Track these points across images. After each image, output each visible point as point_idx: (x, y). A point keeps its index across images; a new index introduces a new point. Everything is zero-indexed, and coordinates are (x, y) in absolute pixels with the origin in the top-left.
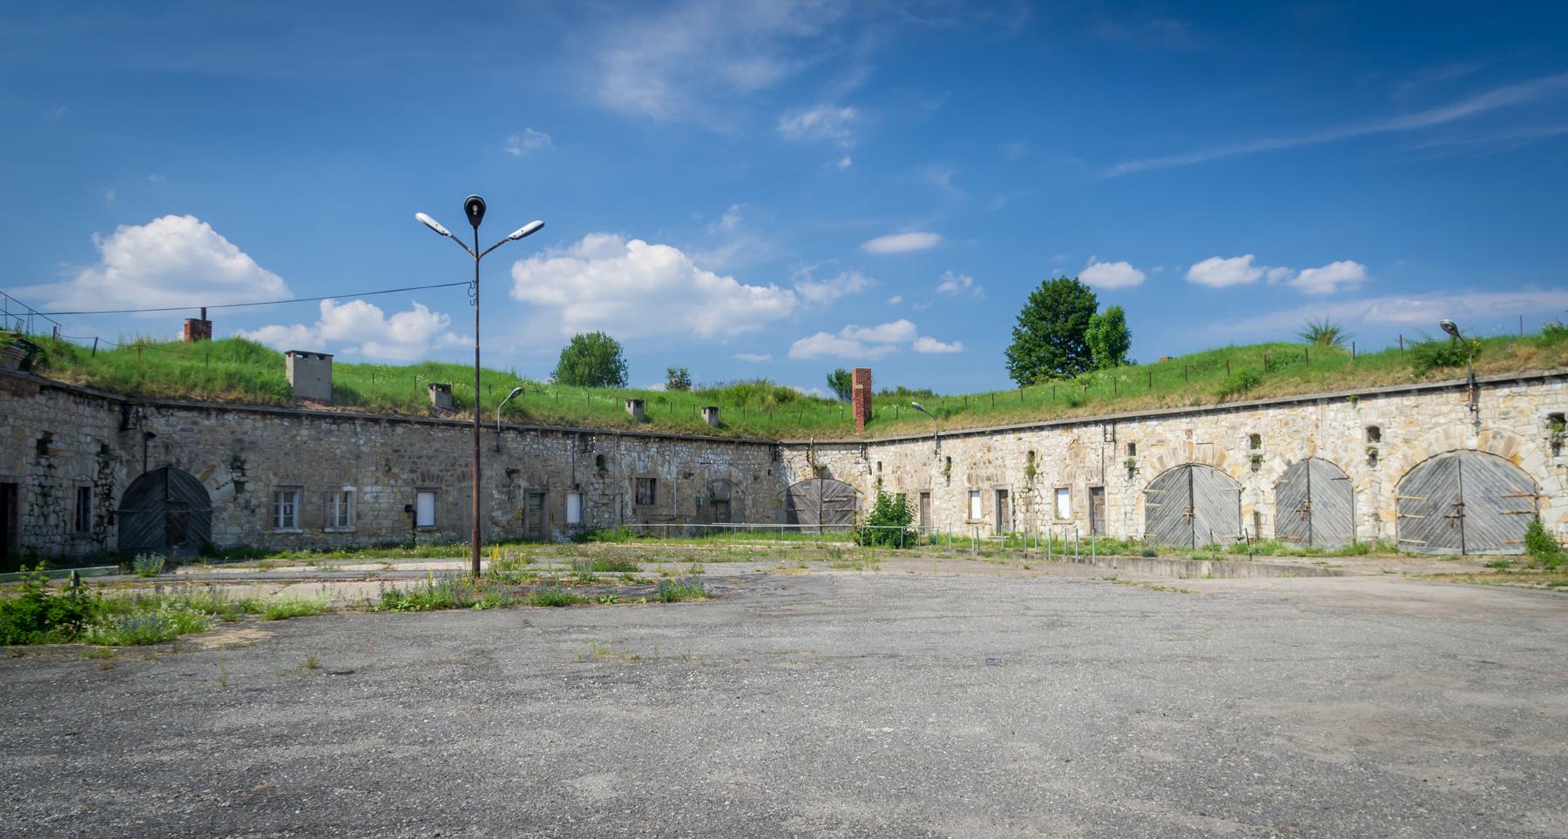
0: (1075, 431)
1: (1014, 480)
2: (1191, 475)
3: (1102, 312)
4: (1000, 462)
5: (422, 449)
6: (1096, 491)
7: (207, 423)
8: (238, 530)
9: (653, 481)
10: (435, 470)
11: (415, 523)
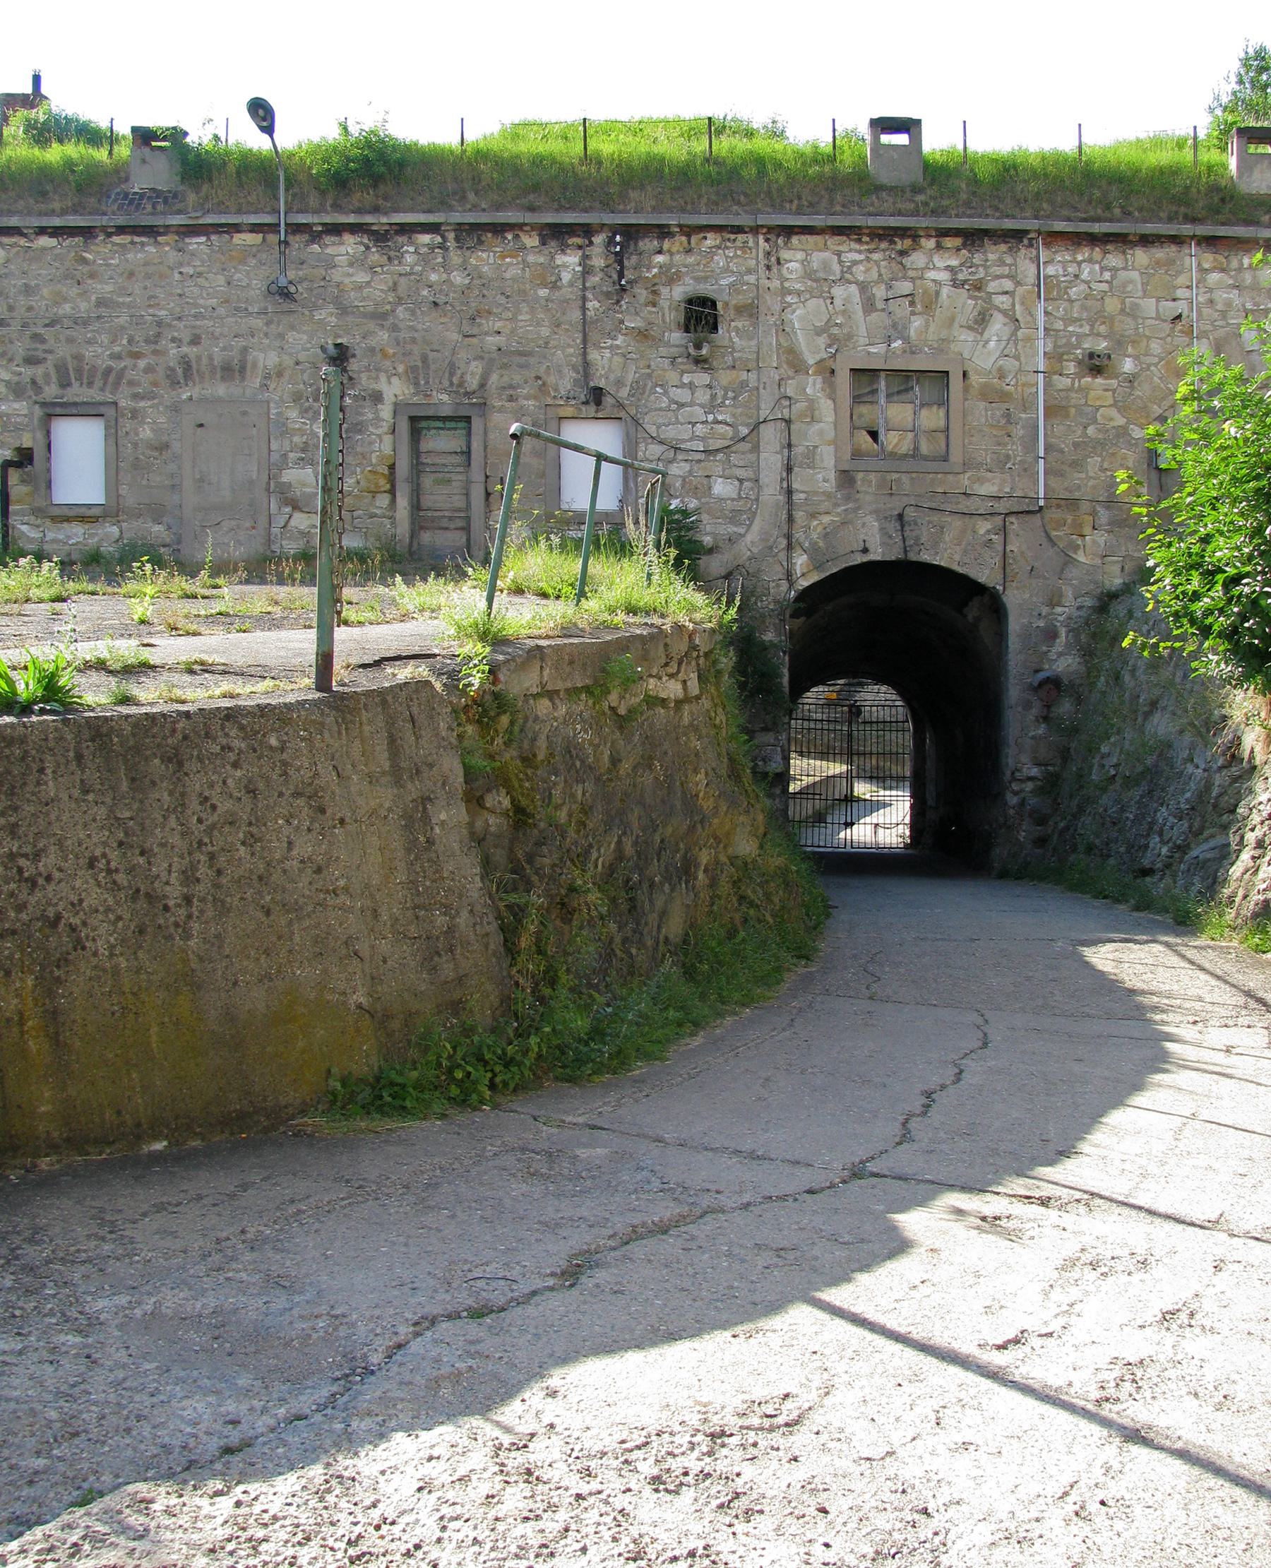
5: (60, 299)
10: (98, 354)
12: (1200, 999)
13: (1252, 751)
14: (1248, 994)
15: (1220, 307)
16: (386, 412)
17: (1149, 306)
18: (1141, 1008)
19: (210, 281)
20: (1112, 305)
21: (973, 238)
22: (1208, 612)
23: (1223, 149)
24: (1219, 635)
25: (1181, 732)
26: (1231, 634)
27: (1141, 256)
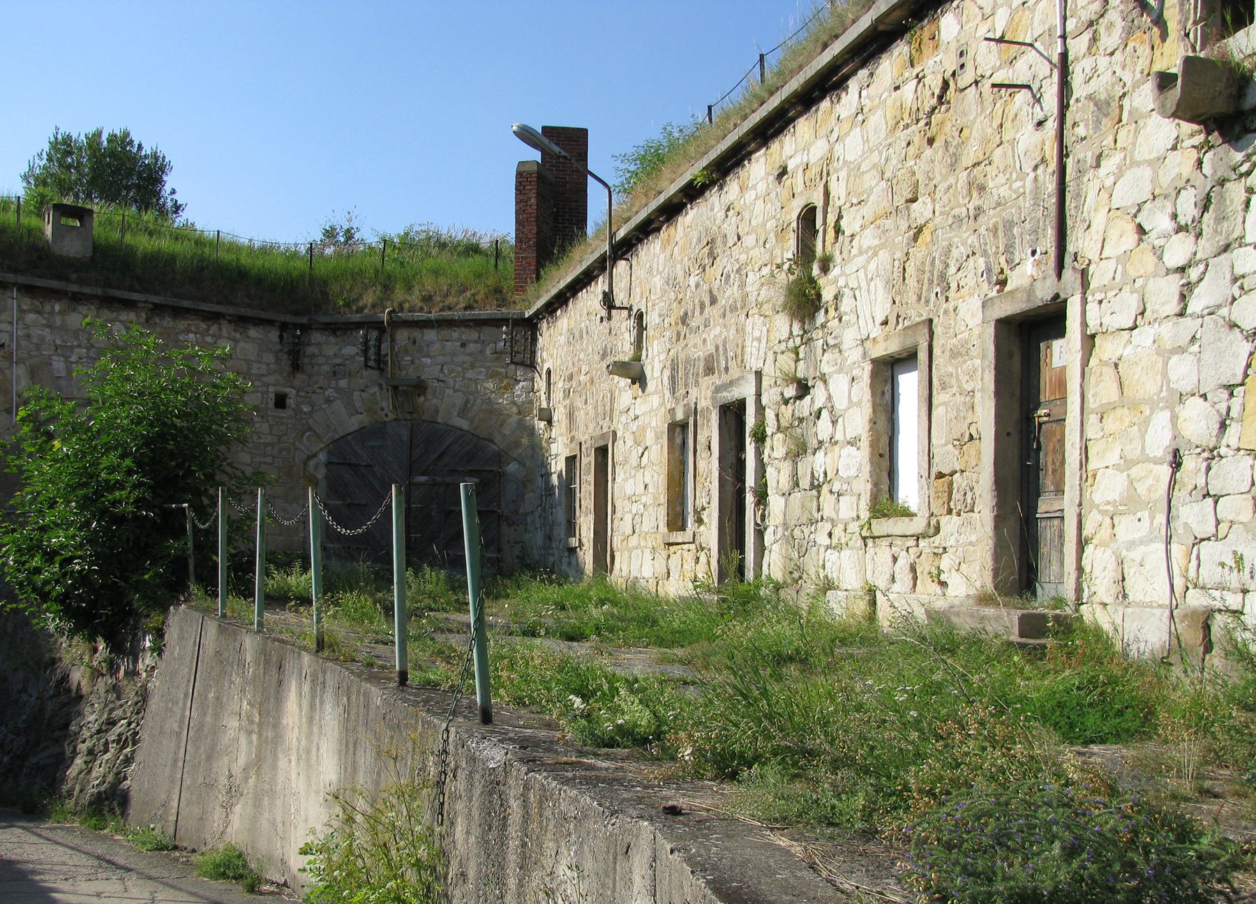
6: (1027, 335)
12: (64, 864)
13: (79, 684)
14: (99, 858)
15: (35, 340)
18: (21, 872)
22: (46, 582)
23: (40, 215)
24: (55, 600)
25: (16, 670)
26: (63, 599)
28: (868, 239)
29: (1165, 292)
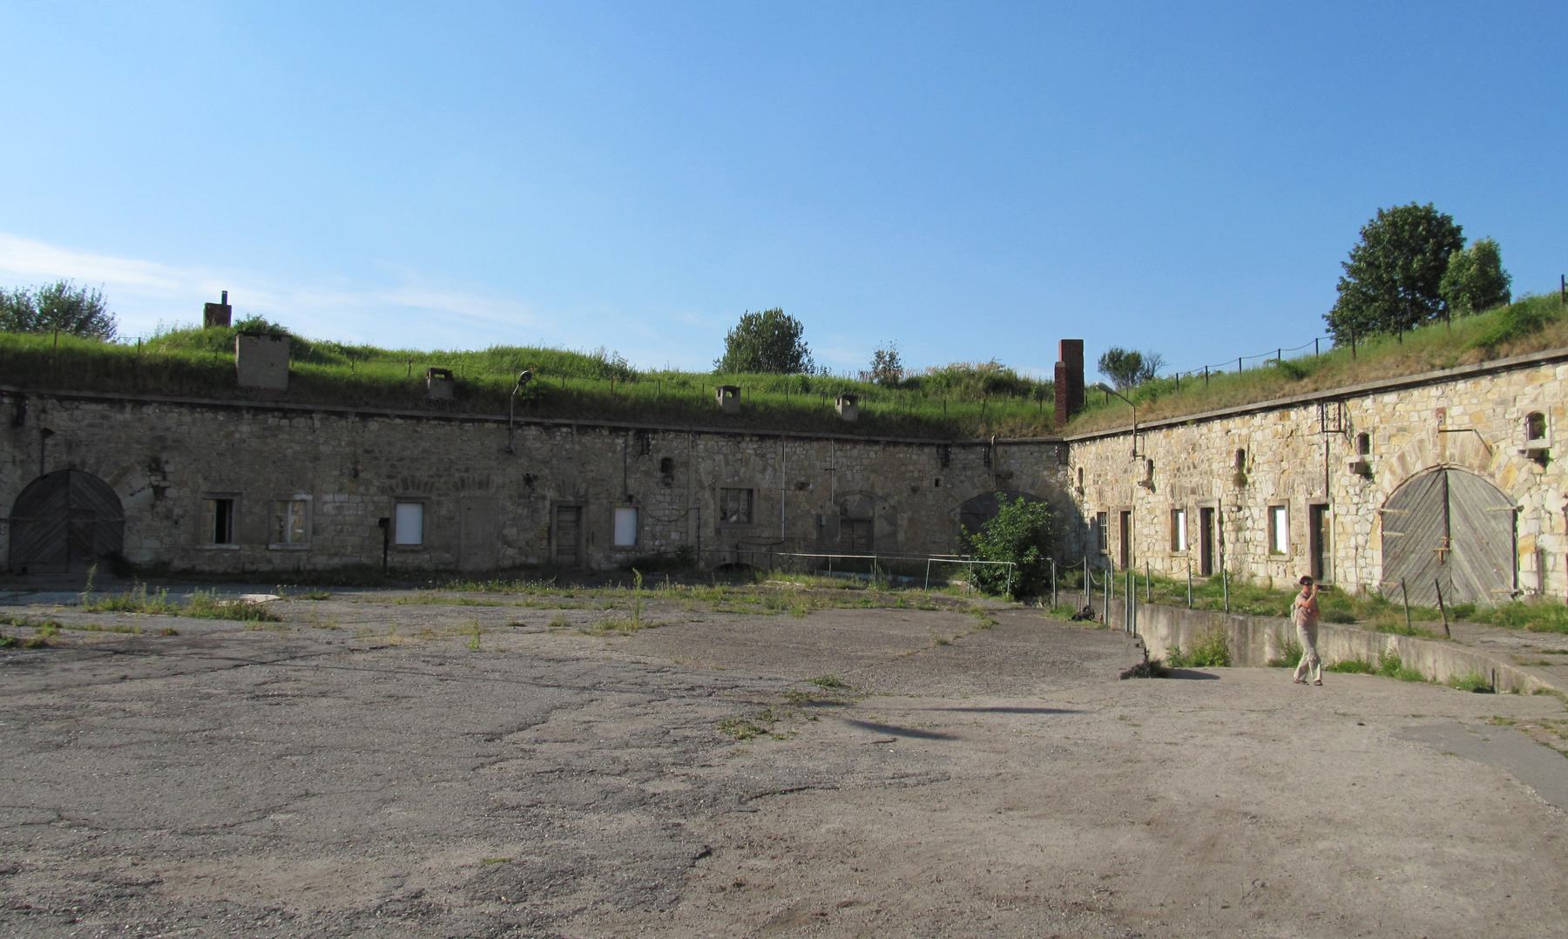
0: (1293, 413)
1: (1221, 492)
2: (1446, 485)
3: (1469, 248)
4: (1205, 466)
6: (1317, 511)
7: (120, 417)
8: (155, 544)
9: (750, 492)
11: (386, 542)
16: (547, 503)
17: (818, 464)
19: (472, 443)
20: (806, 463)
21: (762, 438)
27: (815, 445)
28: (1266, 467)
29: (1353, 509)
